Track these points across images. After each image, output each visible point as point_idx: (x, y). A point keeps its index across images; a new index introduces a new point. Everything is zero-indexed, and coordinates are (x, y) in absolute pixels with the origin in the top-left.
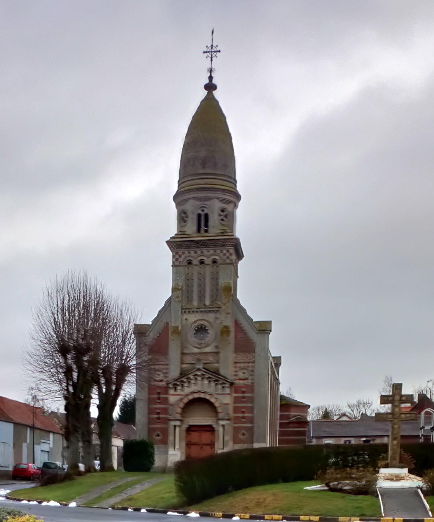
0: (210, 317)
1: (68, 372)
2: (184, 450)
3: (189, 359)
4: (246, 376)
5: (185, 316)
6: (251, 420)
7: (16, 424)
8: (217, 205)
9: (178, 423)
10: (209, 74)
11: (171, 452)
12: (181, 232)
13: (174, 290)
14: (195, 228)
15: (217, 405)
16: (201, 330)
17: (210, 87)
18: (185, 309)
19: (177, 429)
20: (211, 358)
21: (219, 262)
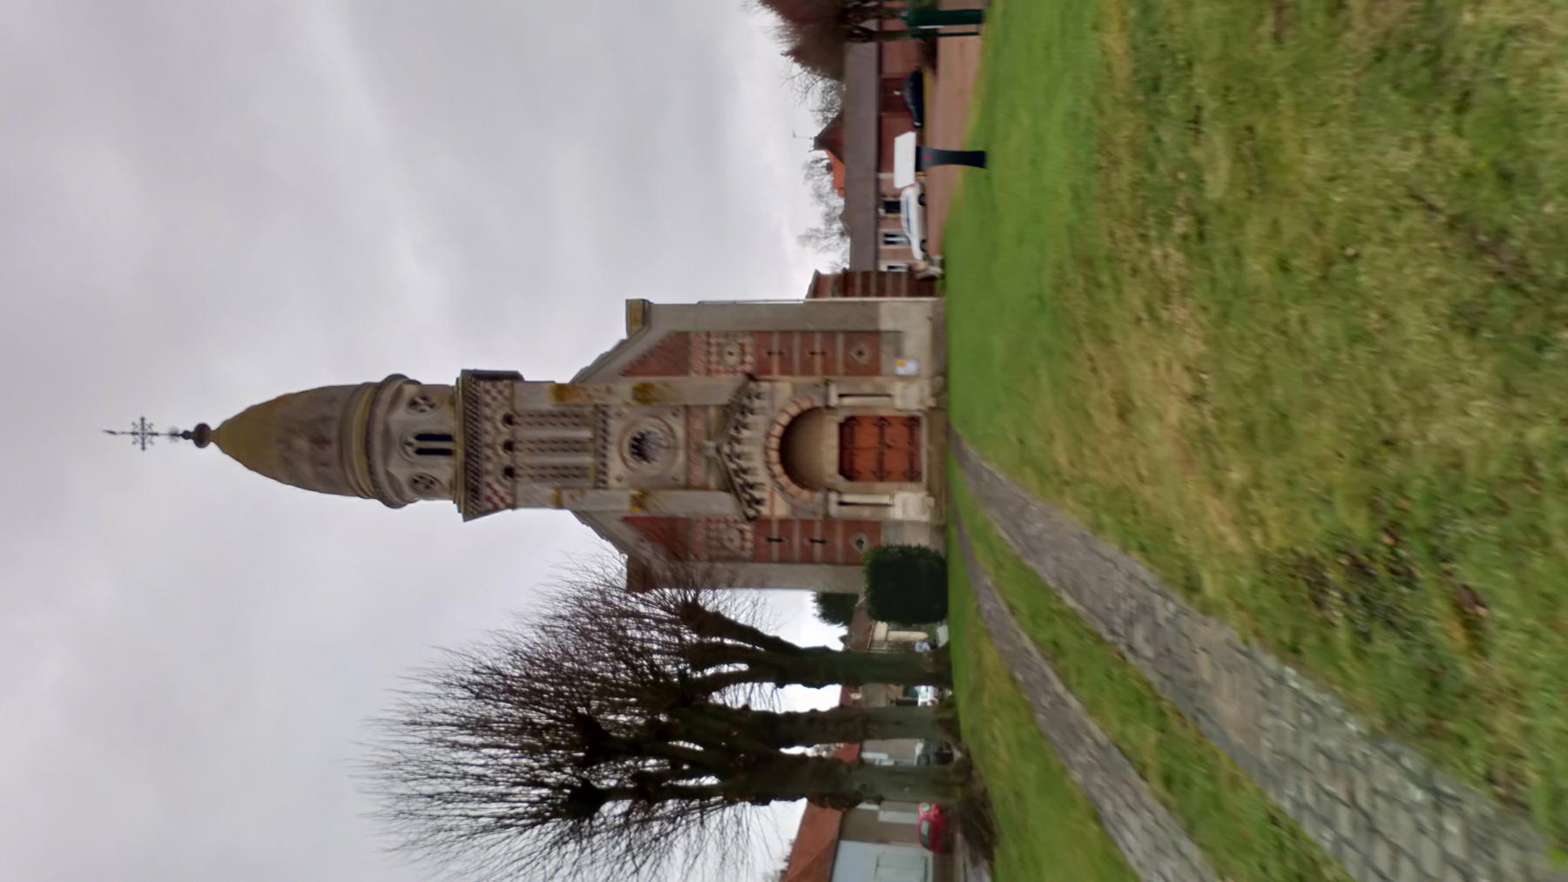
0: (615, 426)
1: (647, 792)
2: (894, 485)
3: (699, 473)
4: (735, 349)
5: (612, 482)
6: (829, 335)
7: (842, 834)
8: (401, 415)
9: (833, 497)
10: (181, 440)
11: (897, 513)
12: (450, 492)
13: (559, 505)
14: (442, 460)
15: (794, 410)
16: (639, 448)
17: (201, 436)
19: (848, 498)
20: (698, 425)
21: (507, 410)
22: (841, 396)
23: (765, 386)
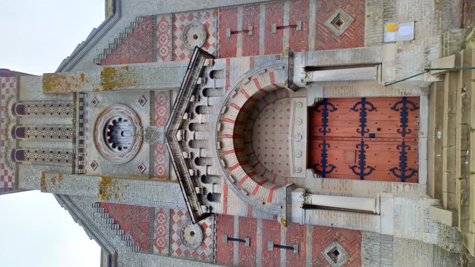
0: (92, 113)
2: (380, 185)
4: (199, 32)
9: (298, 198)
11: (384, 225)
15: (252, 90)
18: (74, 166)
19: (315, 200)
22: (308, 69)
23: (220, 63)
